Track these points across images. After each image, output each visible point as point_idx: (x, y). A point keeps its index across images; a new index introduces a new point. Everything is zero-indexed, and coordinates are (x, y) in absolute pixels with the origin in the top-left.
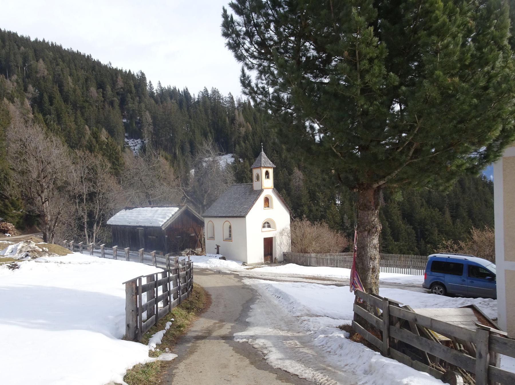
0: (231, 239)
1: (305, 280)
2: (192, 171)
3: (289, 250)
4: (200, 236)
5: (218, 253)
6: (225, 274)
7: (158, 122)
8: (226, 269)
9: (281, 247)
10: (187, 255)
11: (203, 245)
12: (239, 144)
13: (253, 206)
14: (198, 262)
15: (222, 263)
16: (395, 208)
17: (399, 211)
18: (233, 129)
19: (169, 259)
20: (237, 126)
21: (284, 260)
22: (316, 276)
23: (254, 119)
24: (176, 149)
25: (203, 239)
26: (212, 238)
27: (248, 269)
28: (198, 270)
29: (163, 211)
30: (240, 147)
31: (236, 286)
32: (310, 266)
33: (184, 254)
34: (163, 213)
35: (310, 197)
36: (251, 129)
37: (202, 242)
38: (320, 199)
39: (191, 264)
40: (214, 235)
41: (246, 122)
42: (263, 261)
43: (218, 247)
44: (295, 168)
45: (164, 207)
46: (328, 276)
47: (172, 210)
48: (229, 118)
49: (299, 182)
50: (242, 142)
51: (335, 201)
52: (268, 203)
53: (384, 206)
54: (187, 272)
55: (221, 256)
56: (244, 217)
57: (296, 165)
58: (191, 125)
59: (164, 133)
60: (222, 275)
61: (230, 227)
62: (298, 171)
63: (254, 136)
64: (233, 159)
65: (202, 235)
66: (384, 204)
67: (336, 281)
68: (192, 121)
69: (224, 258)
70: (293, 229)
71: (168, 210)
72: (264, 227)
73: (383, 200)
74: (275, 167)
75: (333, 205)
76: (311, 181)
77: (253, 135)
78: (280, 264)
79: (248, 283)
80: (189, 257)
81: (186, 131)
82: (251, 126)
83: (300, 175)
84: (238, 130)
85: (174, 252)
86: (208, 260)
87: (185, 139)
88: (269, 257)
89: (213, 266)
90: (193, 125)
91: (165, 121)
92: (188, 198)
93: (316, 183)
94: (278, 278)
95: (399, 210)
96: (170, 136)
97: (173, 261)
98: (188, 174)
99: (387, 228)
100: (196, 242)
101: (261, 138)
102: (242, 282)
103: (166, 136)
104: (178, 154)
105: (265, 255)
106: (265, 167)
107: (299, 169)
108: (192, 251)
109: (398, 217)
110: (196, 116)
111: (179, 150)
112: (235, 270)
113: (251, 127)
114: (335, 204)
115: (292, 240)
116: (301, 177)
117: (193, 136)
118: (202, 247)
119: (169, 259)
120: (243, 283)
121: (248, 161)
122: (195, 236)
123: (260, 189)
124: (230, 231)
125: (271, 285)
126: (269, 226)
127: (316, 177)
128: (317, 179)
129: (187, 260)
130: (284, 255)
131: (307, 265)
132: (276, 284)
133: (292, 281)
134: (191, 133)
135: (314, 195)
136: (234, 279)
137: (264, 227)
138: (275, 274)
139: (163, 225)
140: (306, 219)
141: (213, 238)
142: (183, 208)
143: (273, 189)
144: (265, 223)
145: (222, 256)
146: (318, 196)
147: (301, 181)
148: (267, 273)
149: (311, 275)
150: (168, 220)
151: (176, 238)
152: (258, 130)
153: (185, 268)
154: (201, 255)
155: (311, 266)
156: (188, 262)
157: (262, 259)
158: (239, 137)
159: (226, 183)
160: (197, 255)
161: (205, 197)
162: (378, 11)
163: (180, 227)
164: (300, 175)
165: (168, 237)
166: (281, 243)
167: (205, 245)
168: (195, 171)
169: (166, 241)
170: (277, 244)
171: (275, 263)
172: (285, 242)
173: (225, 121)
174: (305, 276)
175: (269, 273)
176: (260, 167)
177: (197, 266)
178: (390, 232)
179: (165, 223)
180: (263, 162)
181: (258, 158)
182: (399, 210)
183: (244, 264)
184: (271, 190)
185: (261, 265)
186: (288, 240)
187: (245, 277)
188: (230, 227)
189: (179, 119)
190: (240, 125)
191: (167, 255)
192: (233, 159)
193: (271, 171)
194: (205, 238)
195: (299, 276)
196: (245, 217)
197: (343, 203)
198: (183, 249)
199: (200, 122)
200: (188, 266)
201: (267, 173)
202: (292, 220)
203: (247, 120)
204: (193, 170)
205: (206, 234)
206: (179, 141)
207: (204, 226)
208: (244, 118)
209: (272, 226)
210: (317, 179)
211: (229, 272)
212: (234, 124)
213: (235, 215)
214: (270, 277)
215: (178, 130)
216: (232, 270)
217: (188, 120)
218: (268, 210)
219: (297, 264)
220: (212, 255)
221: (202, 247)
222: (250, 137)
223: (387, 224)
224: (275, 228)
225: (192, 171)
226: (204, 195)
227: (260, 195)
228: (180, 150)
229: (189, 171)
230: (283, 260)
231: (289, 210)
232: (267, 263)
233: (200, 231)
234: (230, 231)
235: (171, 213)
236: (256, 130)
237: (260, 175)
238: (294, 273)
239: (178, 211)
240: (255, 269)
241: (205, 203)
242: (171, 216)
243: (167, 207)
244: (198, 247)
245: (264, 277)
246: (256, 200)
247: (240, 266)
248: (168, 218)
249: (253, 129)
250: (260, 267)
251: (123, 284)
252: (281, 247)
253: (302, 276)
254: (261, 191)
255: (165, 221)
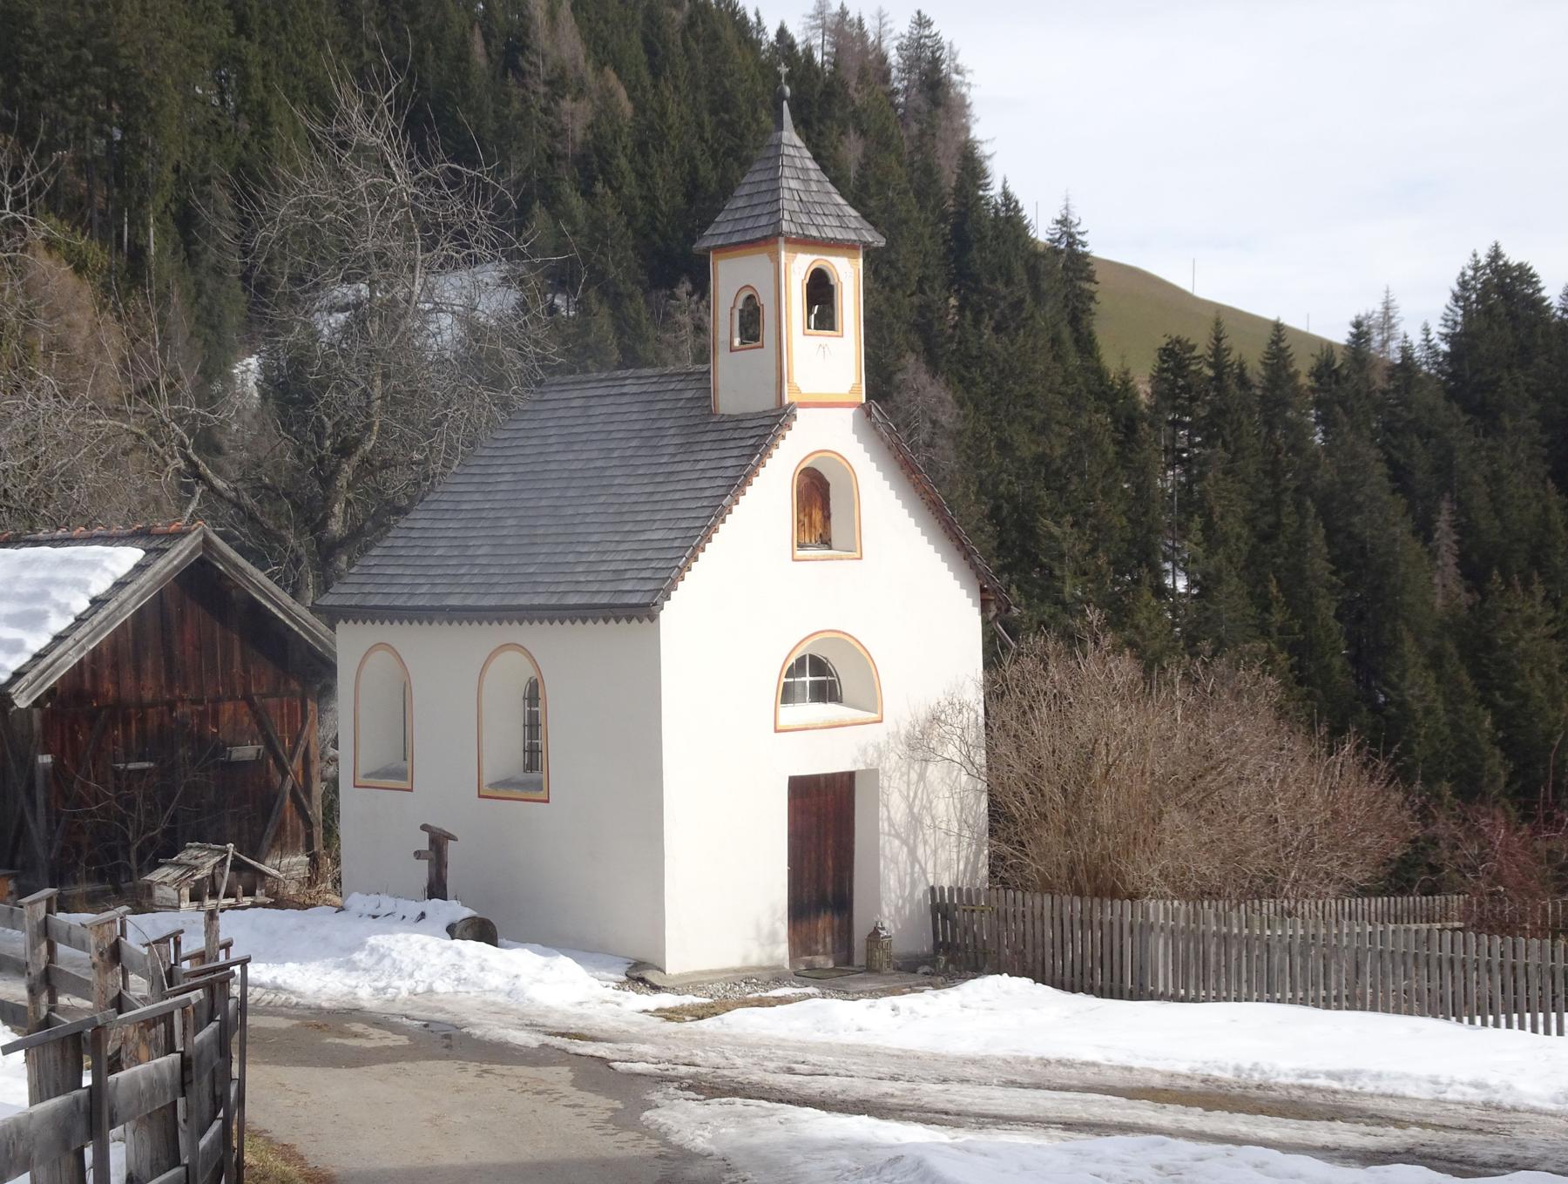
0: (538, 786)
1: (1144, 1112)
2: (249, 369)
3: (975, 871)
4: (297, 764)
5: (437, 889)
6: (498, 1053)
7: (33, 49)
8: (501, 1011)
9: (912, 852)
10: (196, 897)
11: (318, 832)
12: (552, 200)
13: (712, 529)
14: (279, 958)
15: (470, 970)
16: (1530, 623)
17: (1555, 645)
18: (516, 105)
19: (46, 931)
20: (542, 89)
21: (938, 946)
22: (1228, 1076)
23: (650, 50)
24: (146, 228)
25: (318, 788)
26: (397, 774)
27: (670, 1015)
28: (282, 1023)
29: (27, 575)
30: (556, 218)
31: (605, 1164)
32: (1140, 993)
33: (169, 892)
34: (20, 589)
35: (1002, 544)
36: (627, 108)
37: (317, 811)
38: (1062, 555)
39: (225, 982)
40: (406, 752)
41: (599, 67)
42: (781, 952)
43: (438, 841)
44: (910, 359)
45: (37, 543)
46: (1322, 1082)
47: (93, 565)
48: (487, 37)
49: (929, 445)
50: (567, 189)
51: (1158, 574)
52: (827, 517)
53: (1464, 613)
54: (186, 1063)
55: (457, 911)
56: (646, 612)
57: (914, 337)
58: (245, 78)
59: (73, 120)
60: (473, 1068)
61: (533, 694)
62: (924, 378)
63: (645, 155)
64: (513, 296)
65: (314, 752)
66: (1465, 599)
67: (1399, 1123)
68: (251, 50)
69: (483, 931)
70: (1008, 714)
71: (67, 562)
72: (788, 695)
73: (1452, 570)
74: (882, 242)
75: (1147, 595)
76: (1004, 446)
77: (641, 146)
78: (911, 979)
79: (700, 1140)
80: (212, 915)
81: (212, 114)
82: (631, 90)
83: (941, 401)
84: (546, 111)
85: (101, 876)
86: (361, 945)
87: (206, 162)
88: (824, 923)
89: (403, 987)
90: (256, 71)
91: (81, 44)
92: (220, 483)
93: (1040, 460)
94: (931, 1093)
95: (1555, 637)
96: (109, 136)
97: (83, 946)
98: (217, 387)
99: (1487, 748)
100: (267, 803)
101: (695, 169)
102: (647, 1131)
103: (80, 138)
104: (160, 252)
105: (800, 910)
106: (806, 243)
107: (933, 364)
108: (238, 866)
109: (1550, 678)
110: (277, 21)
111: (163, 232)
112: (575, 1025)
113: (631, 98)
114: (1161, 591)
115: (992, 803)
116: (944, 419)
117: (254, 146)
118: (309, 846)
119: (46, 931)
120: (662, 1135)
121: (605, 310)
122: (258, 762)
123: (766, 403)
124: (533, 726)
125: (919, 1164)
126: (826, 692)
127: (1039, 417)
128: (1042, 429)
129: (194, 942)
130: (941, 908)
131: (1112, 990)
132: (937, 1148)
133: (1069, 1126)
134: (245, 126)
135: (1028, 531)
136: (577, 1096)
137: (788, 695)
138: (900, 1056)
139: (18, 675)
140: (1107, 641)
141: (401, 774)
142: (180, 553)
143: (866, 410)
144: (796, 669)
145: (468, 912)
146: (1051, 536)
147: (941, 442)
148: (829, 1049)
149: (1183, 1068)
150: (59, 638)
151: (117, 774)
152: (673, 119)
153: (167, 1018)
154: (303, 907)
155: (1152, 997)
156: (200, 956)
157: (773, 938)
158: (550, 159)
159: (498, 382)
160: (279, 903)
161: (342, 482)
162: (824, 169)
163: (148, 696)
164: (941, 401)
165: (58, 765)
166: (915, 821)
167: (330, 832)
168: (264, 368)
169: (40, 797)
170: (884, 826)
171: (870, 969)
172: (944, 808)
173: (463, 56)
174: (1137, 1081)
175: (849, 1051)
176: (768, 240)
177: (278, 989)
178: (1503, 780)
179: (38, 657)
180: (788, 202)
181: (755, 177)
182: (1555, 637)
183: (640, 974)
184: (848, 414)
185: (767, 985)
186: (971, 799)
187: (662, 1079)
188: (533, 694)
189: (169, 34)
190: (558, 84)
191: (36, 904)
192: (513, 296)
193: (848, 274)
194: (335, 782)
195: (1090, 1075)
196: (653, 618)
197: (1205, 586)
198: (166, 850)
199: (302, 55)
200: (197, 996)
201: (820, 290)
202: (993, 654)
203: (601, 50)
204: (253, 362)
205: (344, 753)
206: (168, 175)
207: (328, 691)
208: (585, 41)
209: (848, 684)
210: (1042, 429)
211: (531, 1040)
212: (520, 73)
213: (573, 600)
214: (860, 1088)
215: (161, 104)
216: (553, 1021)
217: (224, 42)
218: (821, 569)
219: (1040, 978)
220: (387, 903)
221: (309, 846)
222: (623, 162)
223: (1487, 724)
224: (871, 702)
225: (249, 369)
226: (336, 471)
227: (766, 453)
228: (173, 228)
229: (228, 364)
230: (926, 947)
231: (978, 575)
232: (811, 967)
233: (298, 721)
234: (533, 726)
235: (82, 585)
236: (663, 115)
237: (765, 300)
238: (1052, 1055)
239: (140, 568)
240: (727, 1016)
241: (336, 527)
242: (82, 604)
243: (53, 542)
244: (282, 844)
245: (817, 1085)
246: (738, 482)
247: (610, 993)
248: (58, 624)
249: (640, 108)
250: (761, 1003)
251: (424, 827)
252: (912, 852)
253: (1115, 1078)
254: (774, 421)
255: (37, 641)
